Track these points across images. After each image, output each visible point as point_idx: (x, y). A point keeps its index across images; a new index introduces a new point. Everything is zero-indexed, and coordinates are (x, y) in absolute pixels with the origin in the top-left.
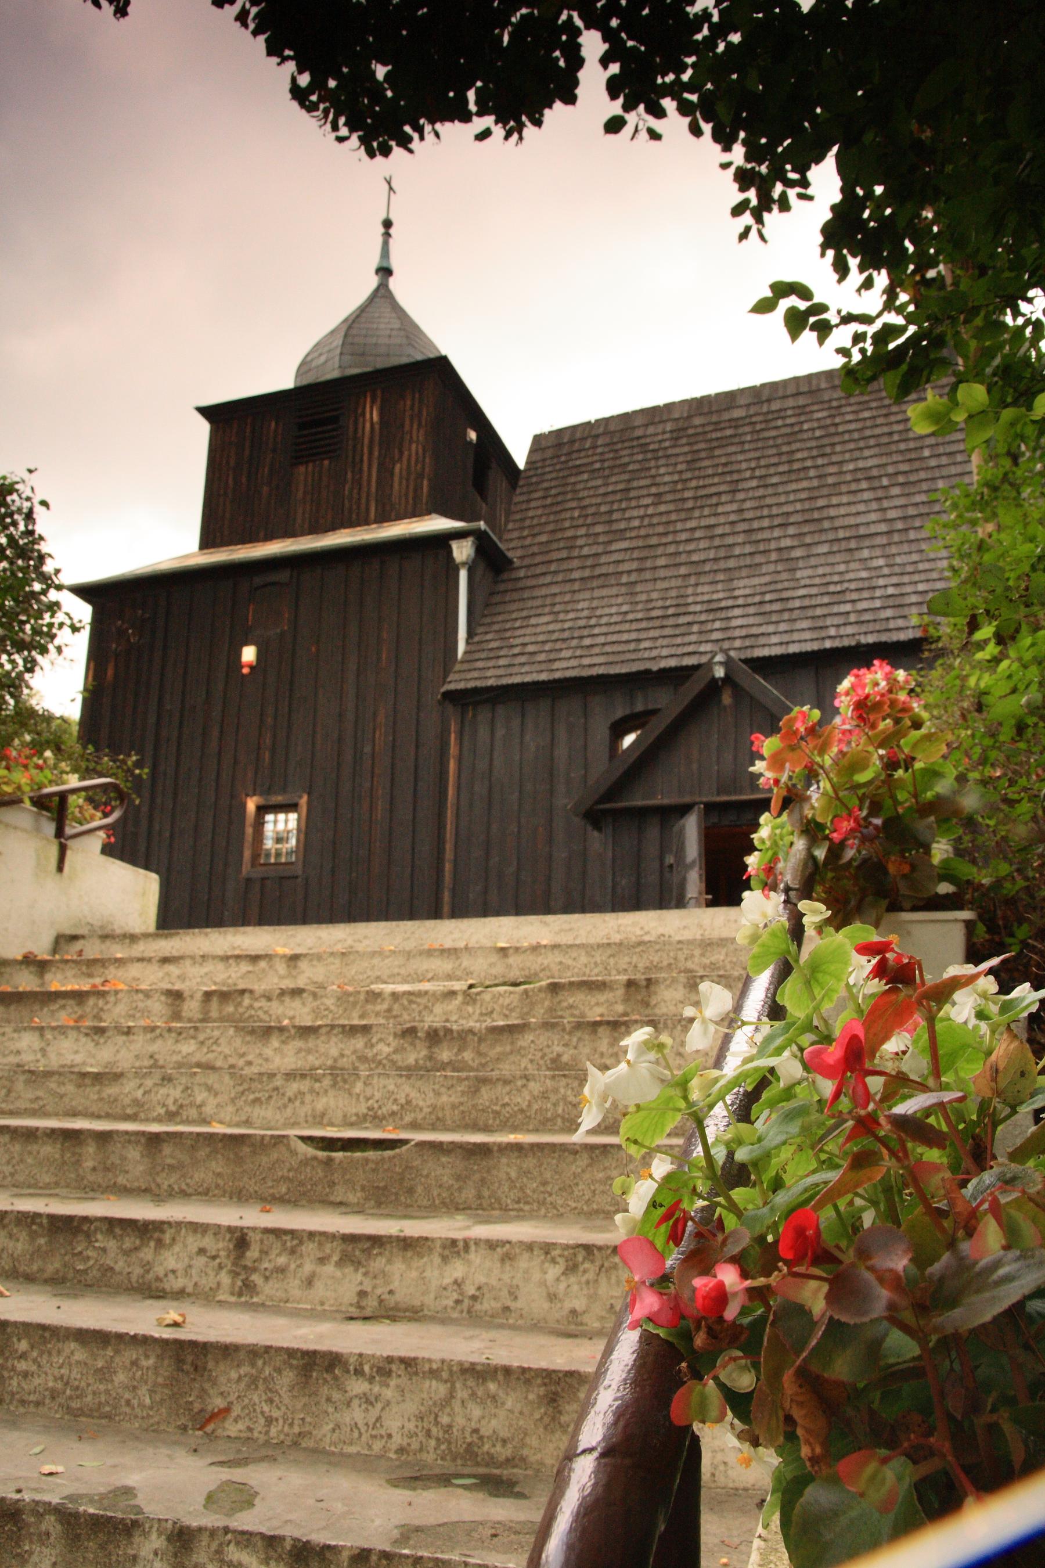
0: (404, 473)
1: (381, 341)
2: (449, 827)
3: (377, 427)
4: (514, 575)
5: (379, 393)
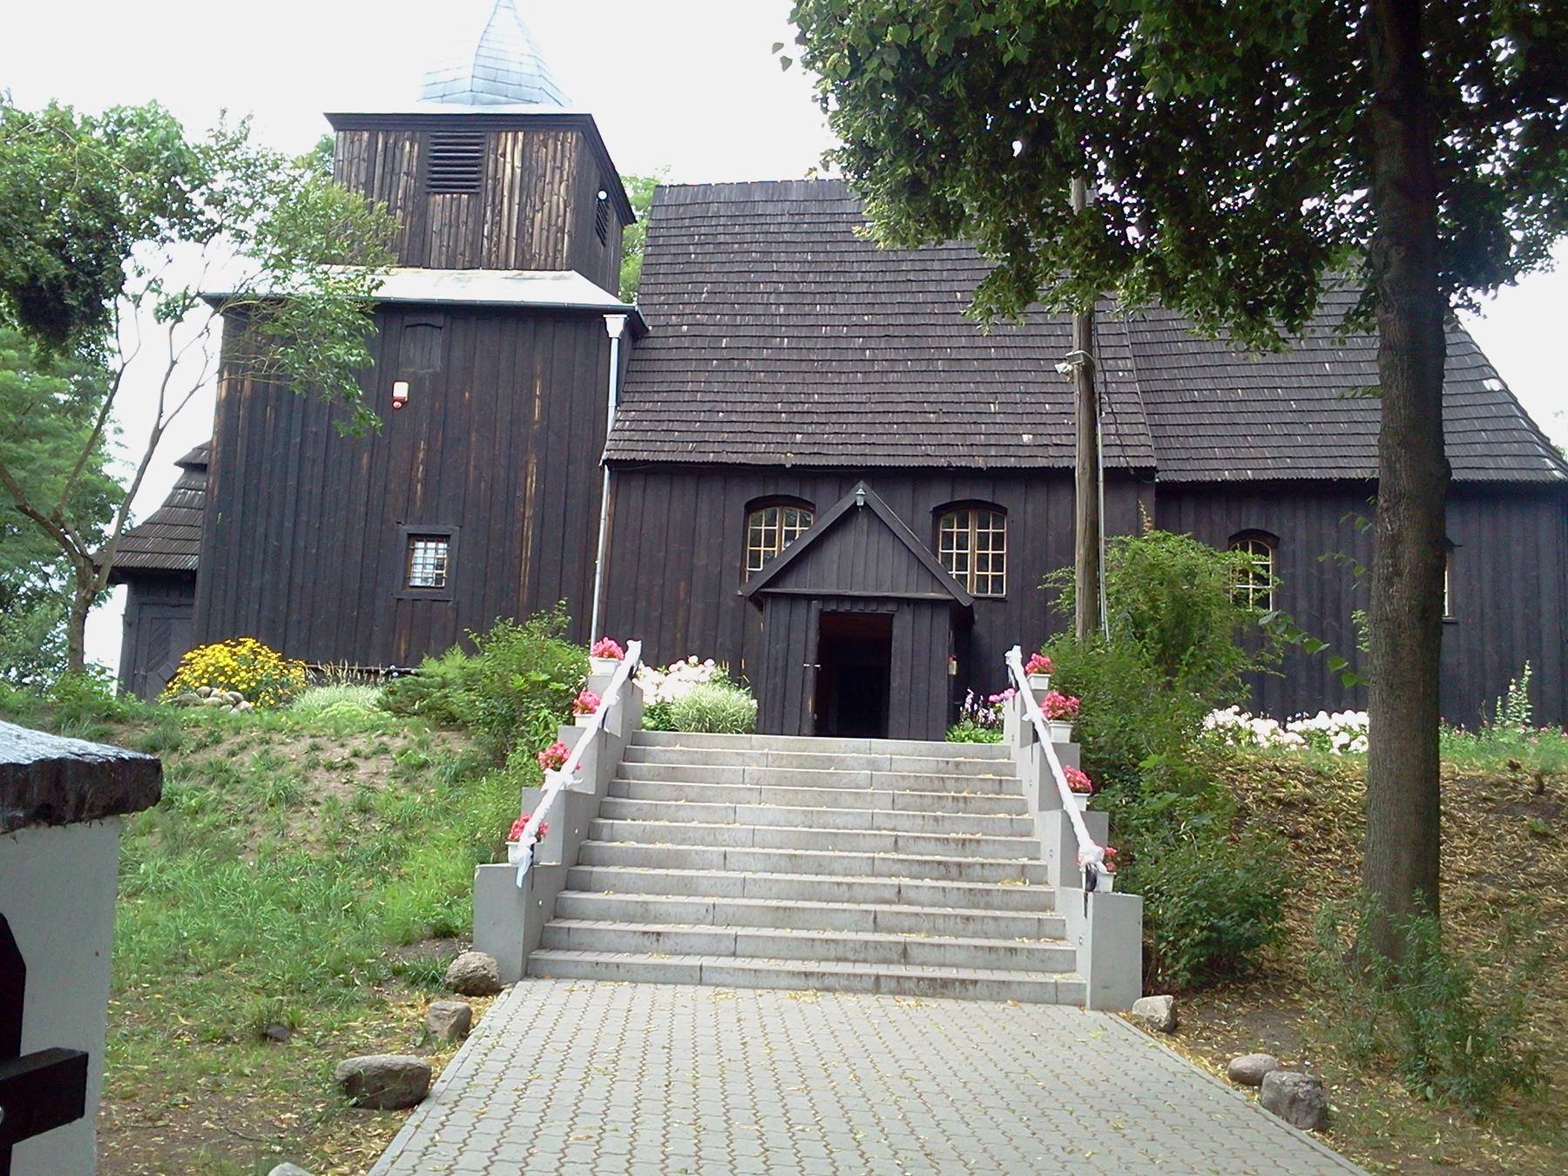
0: (545, 225)
1: (514, 67)
2: (598, 577)
3: (518, 171)
4: (654, 354)
5: (521, 135)
